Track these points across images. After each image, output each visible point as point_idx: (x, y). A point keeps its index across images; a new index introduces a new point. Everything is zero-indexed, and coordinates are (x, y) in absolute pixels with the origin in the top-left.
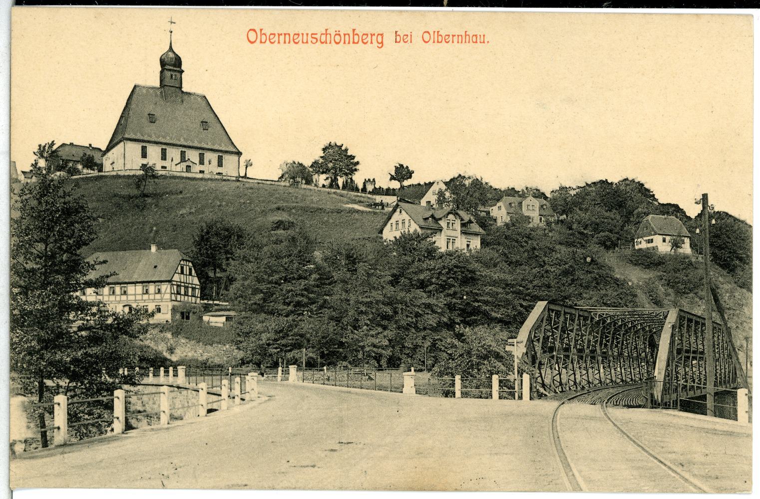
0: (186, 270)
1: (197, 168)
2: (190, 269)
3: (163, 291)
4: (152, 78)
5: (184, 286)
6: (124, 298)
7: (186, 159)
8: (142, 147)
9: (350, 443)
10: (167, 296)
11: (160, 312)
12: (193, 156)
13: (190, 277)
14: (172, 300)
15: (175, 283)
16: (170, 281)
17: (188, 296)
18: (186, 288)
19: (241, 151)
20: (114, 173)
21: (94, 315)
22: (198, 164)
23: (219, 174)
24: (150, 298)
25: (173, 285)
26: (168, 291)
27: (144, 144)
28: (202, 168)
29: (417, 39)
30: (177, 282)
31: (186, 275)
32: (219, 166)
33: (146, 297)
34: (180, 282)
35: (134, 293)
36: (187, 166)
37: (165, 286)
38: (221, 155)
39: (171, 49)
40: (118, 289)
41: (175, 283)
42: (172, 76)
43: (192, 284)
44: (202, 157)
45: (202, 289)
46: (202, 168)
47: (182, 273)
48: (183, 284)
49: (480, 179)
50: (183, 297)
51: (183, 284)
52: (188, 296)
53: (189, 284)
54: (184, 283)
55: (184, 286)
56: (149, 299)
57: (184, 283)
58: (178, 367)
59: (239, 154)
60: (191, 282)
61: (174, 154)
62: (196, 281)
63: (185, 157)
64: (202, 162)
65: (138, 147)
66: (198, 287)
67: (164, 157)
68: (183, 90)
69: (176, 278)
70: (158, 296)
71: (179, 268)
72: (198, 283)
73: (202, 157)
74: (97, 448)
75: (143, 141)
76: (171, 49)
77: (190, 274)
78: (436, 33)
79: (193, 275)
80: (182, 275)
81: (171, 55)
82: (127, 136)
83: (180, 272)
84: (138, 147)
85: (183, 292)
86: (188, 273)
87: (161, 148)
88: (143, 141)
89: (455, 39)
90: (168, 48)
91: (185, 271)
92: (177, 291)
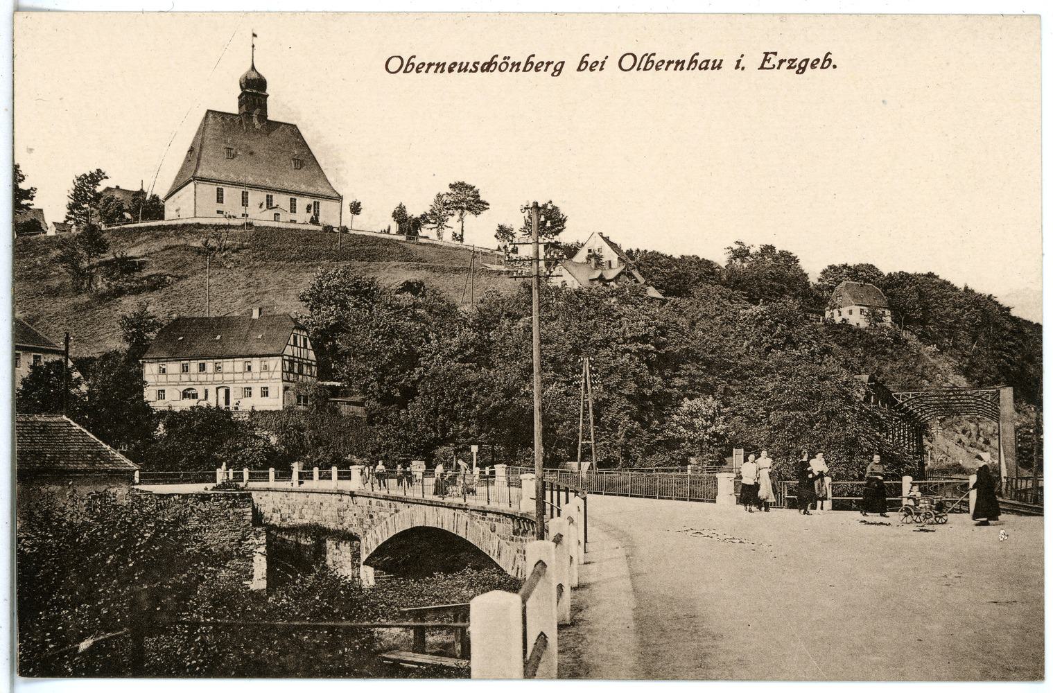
0: (300, 342)
1: (286, 216)
2: (305, 340)
4: (231, 105)
6: (218, 377)
7: (274, 205)
9: (589, 563)
10: (278, 375)
11: (267, 396)
12: (282, 201)
14: (283, 381)
15: (287, 358)
16: (282, 355)
17: (293, 373)
18: (300, 364)
19: (341, 194)
20: (180, 222)
22: (289, 211)
25: (285, 360)
26: (279, 368)
27: (220, 186)
28: (293, 217)
29: (612, 65)
30: (289, 356)
33: (248, 376)
34: (293, 356)
35: (231, 370)
38: (317, 200)
39: (253, 68)
40: (210, 365)
41: (287, 358)
43: (307, 359)
44: (293, 202)
46: (293, 217)
47: (295, 344)
48: (296, 360)
49: (736, 247)
50: (309, 378)
51: (296, 360)
52: (293, 373)
53: (303, 359)
55: (298, 362)
58: (351, 467)
59: (339, 198)
61: (256, 197)
62: (312, 355)
63: (271, 205)
64: (293, 210)
65: (211, 189)
66: (314, 363)
67: (245, 202)
68: (268, 118)
69: (289, 351)
70: (265, 375)
71: (292, 338)
72: (315, 359)
73: (293, 202)
74: (413, 584)
75: (270, 189)
76: (253, 68)
77: (305, 347)
80: (296, 348)
81: (254, 75)
82: (199, 174)
84: (211, 189)
85: (296, 370)
86: (302, 346)
87: (216, 187)
88: (270, 189)
90: (249, 66)
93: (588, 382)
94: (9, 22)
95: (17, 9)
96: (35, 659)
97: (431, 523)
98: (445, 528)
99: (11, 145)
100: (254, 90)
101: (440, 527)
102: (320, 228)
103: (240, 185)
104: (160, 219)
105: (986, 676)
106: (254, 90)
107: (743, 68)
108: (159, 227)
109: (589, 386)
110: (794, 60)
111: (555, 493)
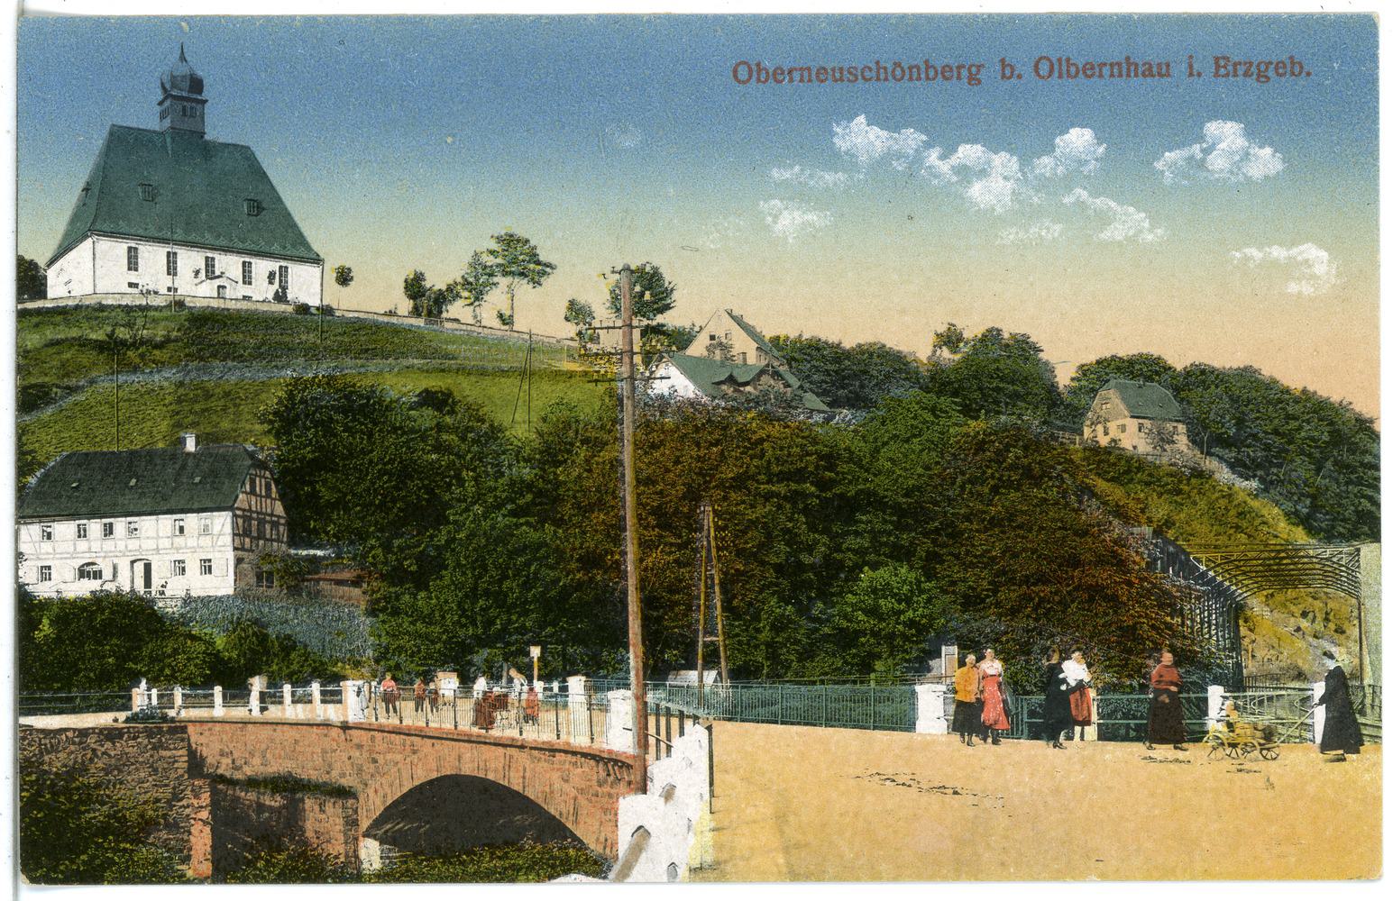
3: (216, 529)
4: (147, 115)
5: (258, 519)
6: (133, 544)
7: (217, 273)
8: (244, 263)
11: (210, 572)
13: (269, 501)
20: (71, 303)
21: (897, 537)
23: (245, 298)
24: (189, 545)
31: (261, 496)
32: (130, 269)
36: (219, 287)
37: (222, 520)
42: (184, 109)
45: (291, 525)
47: (253, 492)
48: (268, 518)
51: (268, 518)
53: (266, 514)
54: (269, 515)
56: (186, 547)
57: (258, 513)
60: (269, 511)
62: (279, 509)
63: (213, 272)
77: (268, 496)
78: (1064, 63)
79: (273, 496)
83: (248, 490)
89: (1106, 71)
91: (258, 489)
92: (244, 529)
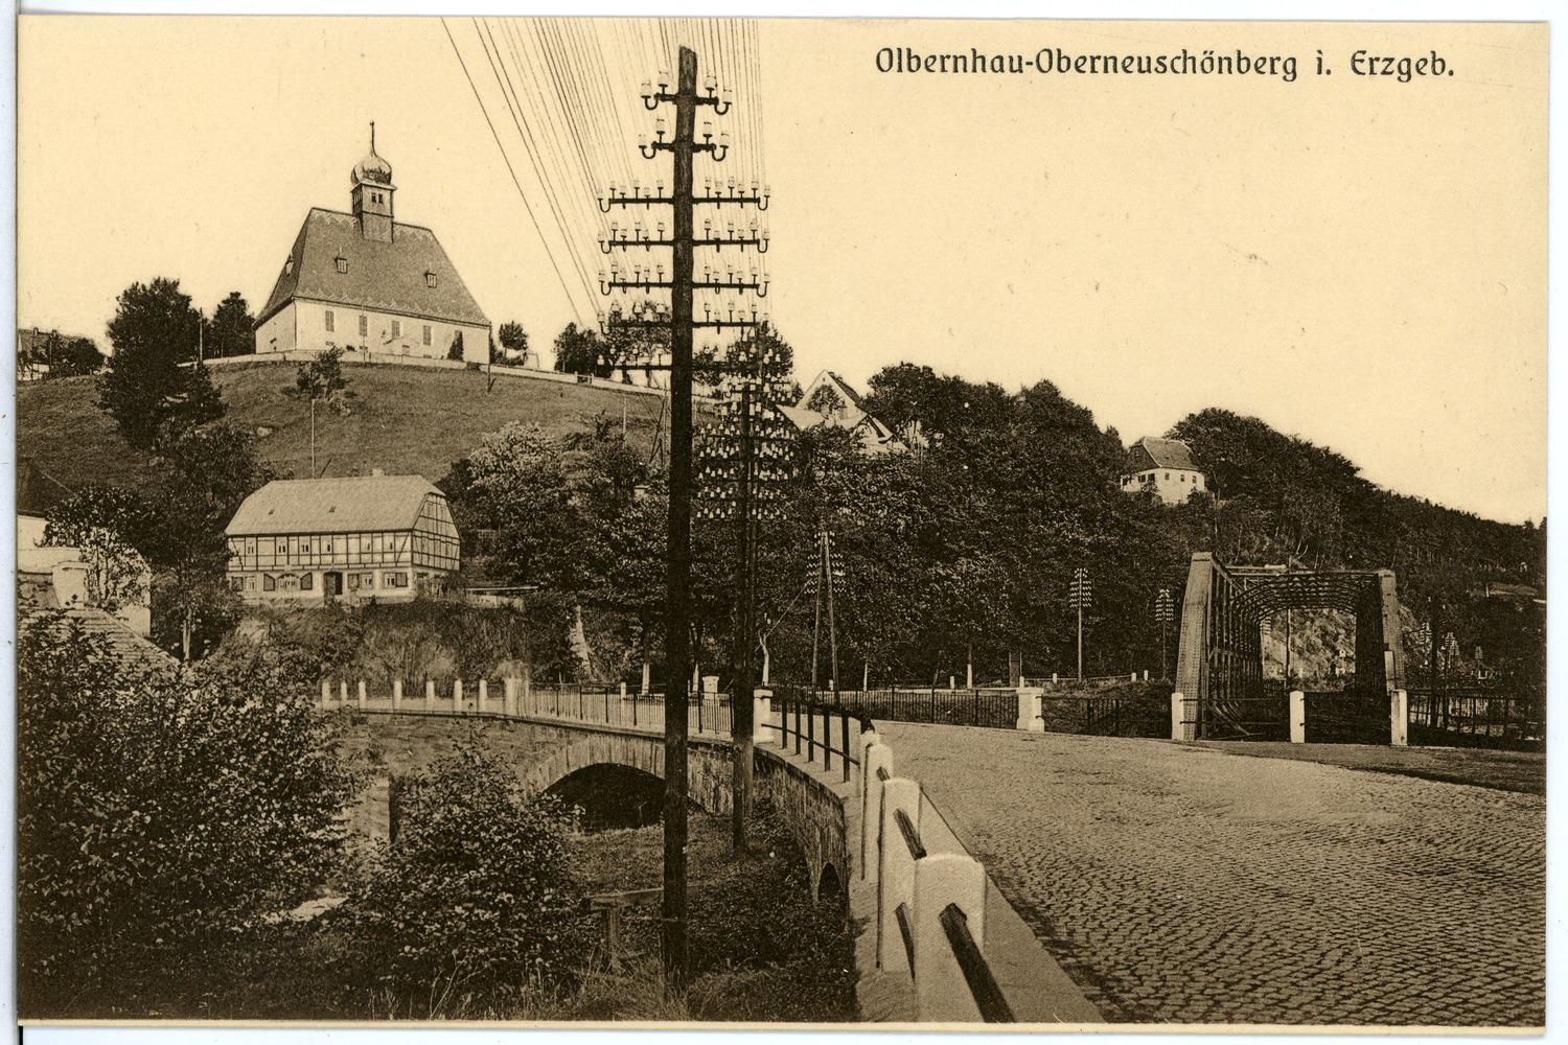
46: (427, 350)
93: (828, 564)
94: (14, 19)
95: (20, 12)
96: (44, 992)
97: (618, 759)
98: (614, 761)
99: (14, 32)
100: (373, 182)
101: (630, 764)
102: (464, 365)
103: (357, 306)
104: (249, 353)
105: (22, 443)
106: (373, 182)
107: (1329, 72)
108: (246, 366)
109: (828, 570)
110: (1391, 60)
111: (804, 718)
